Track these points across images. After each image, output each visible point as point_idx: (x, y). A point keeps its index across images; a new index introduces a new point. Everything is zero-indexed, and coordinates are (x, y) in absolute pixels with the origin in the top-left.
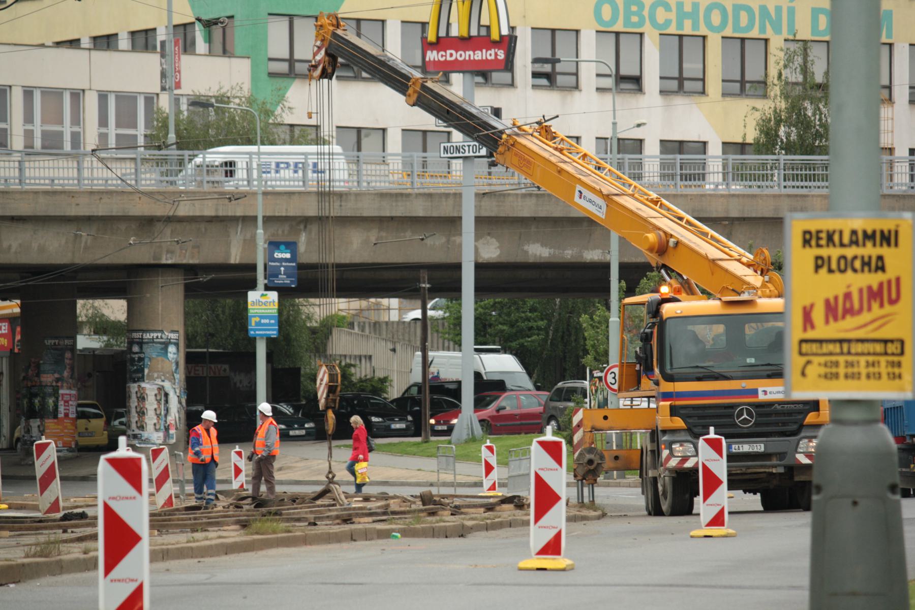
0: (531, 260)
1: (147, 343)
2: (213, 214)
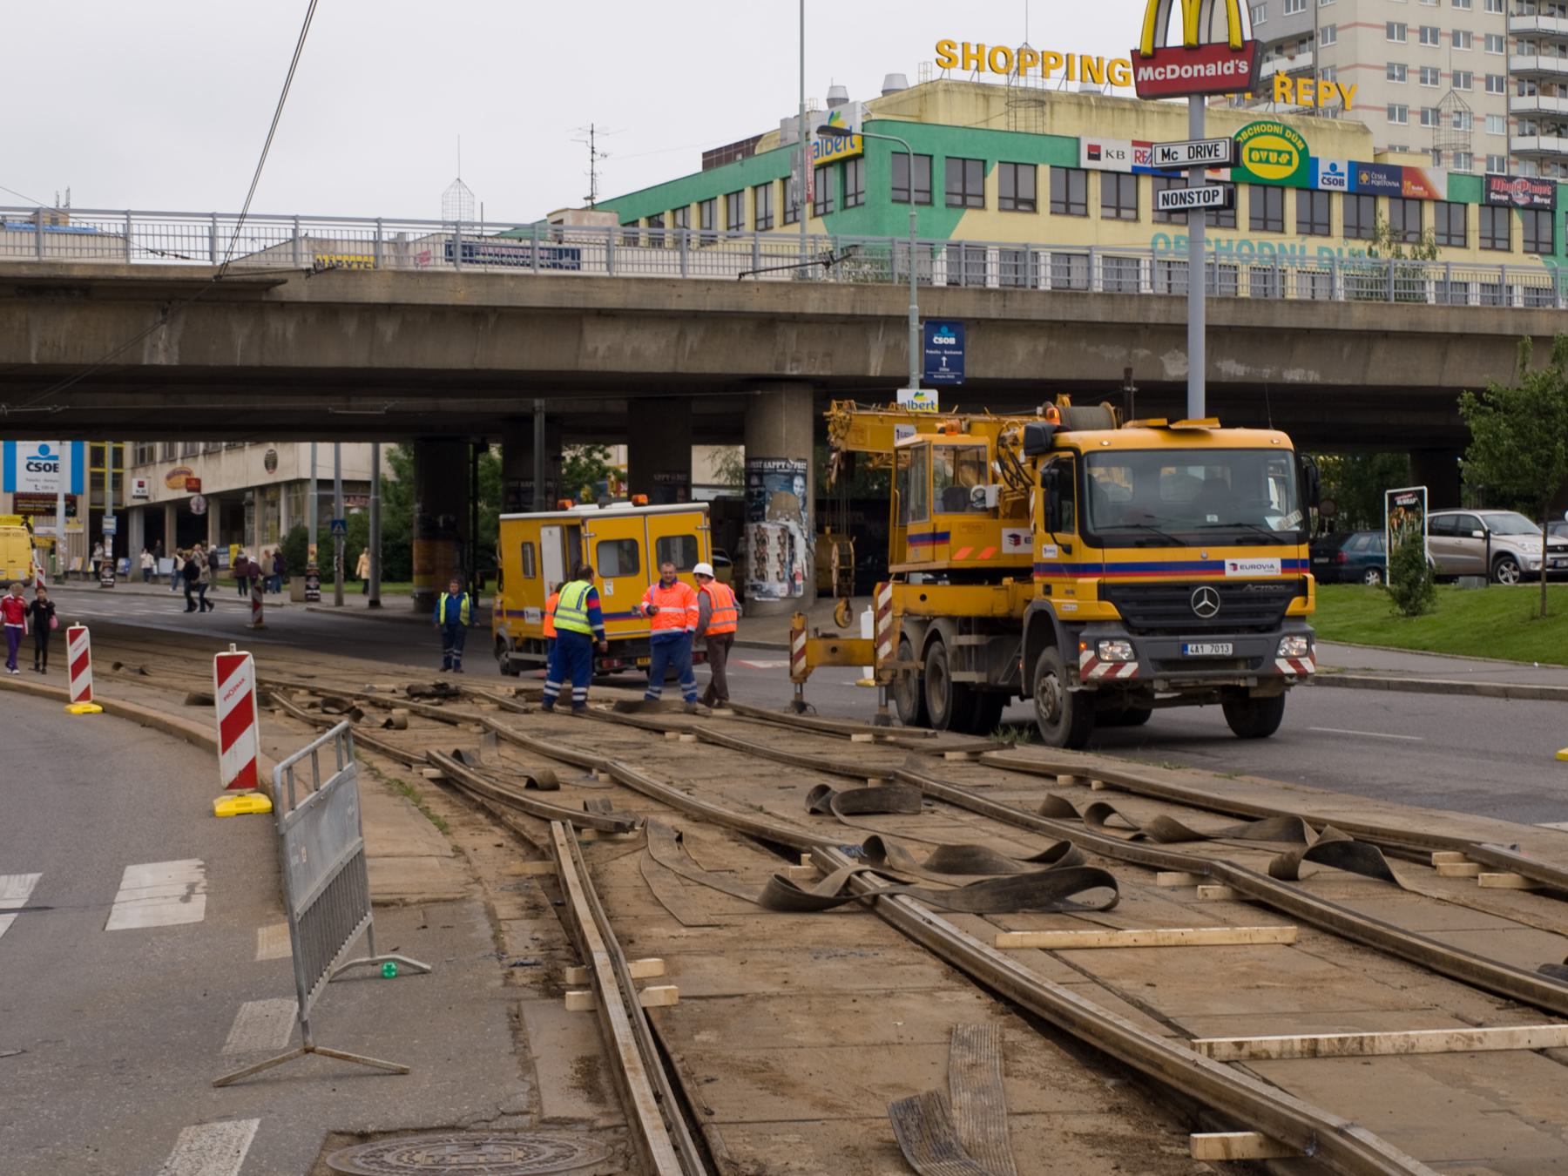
0: (1224, 379)
1: (769, 474)
2: (849, 311)
